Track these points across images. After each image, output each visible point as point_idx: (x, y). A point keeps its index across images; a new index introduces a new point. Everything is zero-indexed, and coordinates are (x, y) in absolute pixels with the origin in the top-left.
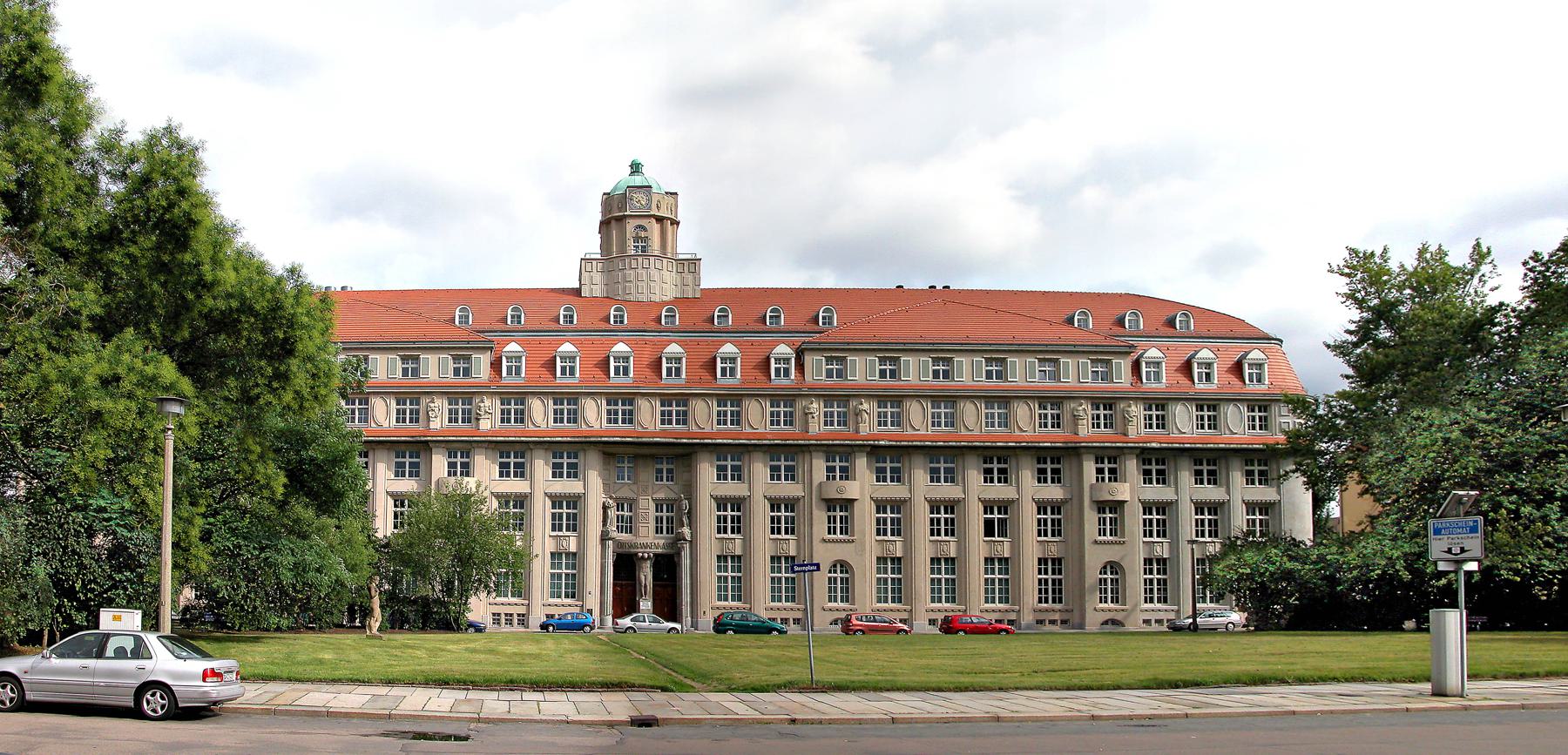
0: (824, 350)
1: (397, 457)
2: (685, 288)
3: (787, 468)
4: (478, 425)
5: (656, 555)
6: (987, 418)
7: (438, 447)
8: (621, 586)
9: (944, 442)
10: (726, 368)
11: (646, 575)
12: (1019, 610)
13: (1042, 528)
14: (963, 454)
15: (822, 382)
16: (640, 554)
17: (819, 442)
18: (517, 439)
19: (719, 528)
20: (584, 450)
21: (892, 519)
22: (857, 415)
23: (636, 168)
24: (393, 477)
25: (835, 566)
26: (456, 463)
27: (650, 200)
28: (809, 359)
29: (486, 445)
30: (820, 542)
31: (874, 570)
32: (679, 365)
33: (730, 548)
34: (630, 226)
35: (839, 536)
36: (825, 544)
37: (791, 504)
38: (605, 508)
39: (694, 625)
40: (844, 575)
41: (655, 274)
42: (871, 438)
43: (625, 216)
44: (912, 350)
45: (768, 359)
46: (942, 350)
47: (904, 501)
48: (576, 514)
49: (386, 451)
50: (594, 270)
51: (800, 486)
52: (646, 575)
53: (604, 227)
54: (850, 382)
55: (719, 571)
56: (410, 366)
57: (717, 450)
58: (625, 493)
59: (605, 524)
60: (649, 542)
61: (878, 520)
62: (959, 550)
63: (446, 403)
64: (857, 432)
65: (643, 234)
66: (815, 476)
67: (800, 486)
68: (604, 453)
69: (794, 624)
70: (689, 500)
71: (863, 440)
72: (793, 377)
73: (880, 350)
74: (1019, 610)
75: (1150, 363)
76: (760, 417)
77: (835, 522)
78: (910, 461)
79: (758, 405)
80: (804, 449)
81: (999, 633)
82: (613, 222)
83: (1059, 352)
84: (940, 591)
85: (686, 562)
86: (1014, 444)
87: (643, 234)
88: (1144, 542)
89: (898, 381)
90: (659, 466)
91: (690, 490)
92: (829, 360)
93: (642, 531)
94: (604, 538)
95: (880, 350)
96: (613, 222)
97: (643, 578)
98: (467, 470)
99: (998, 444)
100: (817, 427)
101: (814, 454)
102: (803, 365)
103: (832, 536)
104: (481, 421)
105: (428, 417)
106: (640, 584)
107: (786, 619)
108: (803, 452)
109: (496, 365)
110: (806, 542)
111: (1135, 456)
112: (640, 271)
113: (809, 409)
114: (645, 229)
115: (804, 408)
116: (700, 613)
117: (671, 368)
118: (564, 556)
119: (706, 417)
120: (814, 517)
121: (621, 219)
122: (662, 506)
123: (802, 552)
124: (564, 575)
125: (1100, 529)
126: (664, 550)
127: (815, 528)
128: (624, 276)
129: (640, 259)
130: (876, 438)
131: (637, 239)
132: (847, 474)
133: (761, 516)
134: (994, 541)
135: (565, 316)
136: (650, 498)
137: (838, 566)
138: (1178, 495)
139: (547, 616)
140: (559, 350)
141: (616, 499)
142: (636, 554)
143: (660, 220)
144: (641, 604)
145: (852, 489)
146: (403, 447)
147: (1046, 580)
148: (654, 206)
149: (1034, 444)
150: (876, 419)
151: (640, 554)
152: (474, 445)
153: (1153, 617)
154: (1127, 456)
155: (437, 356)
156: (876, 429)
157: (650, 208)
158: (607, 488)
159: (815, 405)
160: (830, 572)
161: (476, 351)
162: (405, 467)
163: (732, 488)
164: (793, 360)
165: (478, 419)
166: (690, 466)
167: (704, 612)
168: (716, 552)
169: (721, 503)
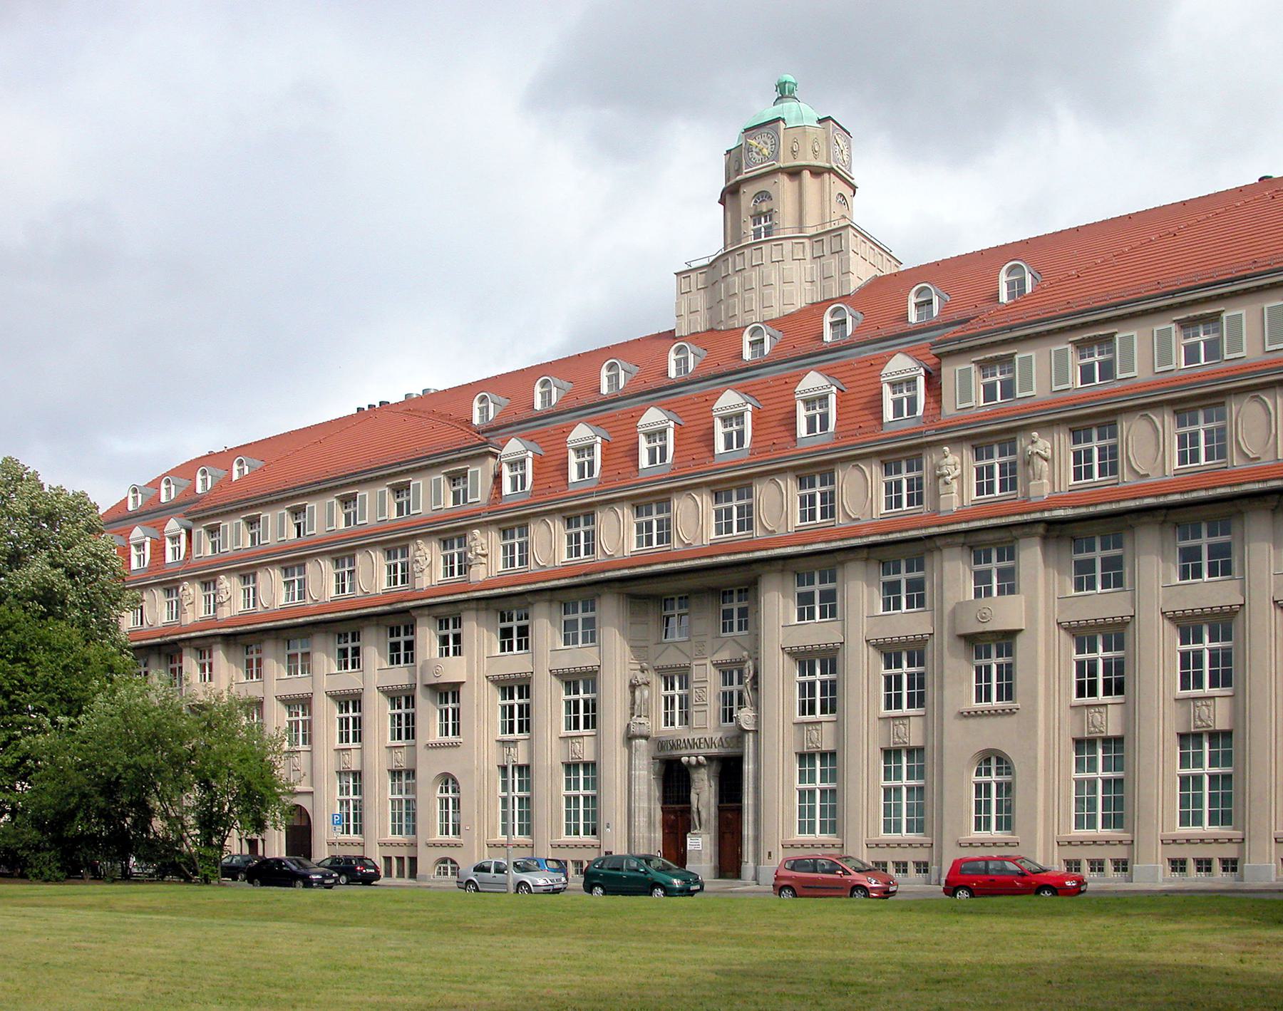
0: (971, 350)
1: (800, 584)
2: (787, 287)
3: (1215, 551)
8: (674, 812)
11: (704, 793)
13: (983, 684)
19: (1184, 677)
28: (950, 373)
29: (865, 553)
30: (955, 718)
33: (577, 751)
36: (965, 721)
37: (916, 650)
44: (1133, 316)
48: (835, 681)
49: (1157, 527)
52: (704, 793)
56: (1201, 338)
58: (671, 658)
63: (968, 454)
69: (1199, 870)
70: (756, 660)
71: (1087, 506)
73: (1073, 328)
79: (267, 574)
80: (929, 544)
81: (1037, 892)
83: (408, 472)
84: (1092, 806)
85: (748, 767)
90: (726, 606)
92: (984, 366)
95: (1073, 328)
96: (806, 174)
98: (1009, 584)
103: (984, 705)
111: (1037, 540)
112: (787, 265)
116: (763, 855)
117: (901, 400)
120: (947, 672)
122: (673, 678)
124: (904, 790)
125: (458, 720)
126: (730, 750)
127: (947, 693)
128: (762, 278)
136: (708, 662)
137: (993, 761)
139: (1068, 862)
140: (571, 438)
141: (658, 670)
144: (688, 839)
146: (573, 594)
147: (400, 801)
151: (684, 759)
153: (1190, 853)
154: (946, 552)
155: (1257, 307)
158: (638, 650)
159: (955, 458)
161: (1122, 325)
163: (819, 632)
167: (770, 853)
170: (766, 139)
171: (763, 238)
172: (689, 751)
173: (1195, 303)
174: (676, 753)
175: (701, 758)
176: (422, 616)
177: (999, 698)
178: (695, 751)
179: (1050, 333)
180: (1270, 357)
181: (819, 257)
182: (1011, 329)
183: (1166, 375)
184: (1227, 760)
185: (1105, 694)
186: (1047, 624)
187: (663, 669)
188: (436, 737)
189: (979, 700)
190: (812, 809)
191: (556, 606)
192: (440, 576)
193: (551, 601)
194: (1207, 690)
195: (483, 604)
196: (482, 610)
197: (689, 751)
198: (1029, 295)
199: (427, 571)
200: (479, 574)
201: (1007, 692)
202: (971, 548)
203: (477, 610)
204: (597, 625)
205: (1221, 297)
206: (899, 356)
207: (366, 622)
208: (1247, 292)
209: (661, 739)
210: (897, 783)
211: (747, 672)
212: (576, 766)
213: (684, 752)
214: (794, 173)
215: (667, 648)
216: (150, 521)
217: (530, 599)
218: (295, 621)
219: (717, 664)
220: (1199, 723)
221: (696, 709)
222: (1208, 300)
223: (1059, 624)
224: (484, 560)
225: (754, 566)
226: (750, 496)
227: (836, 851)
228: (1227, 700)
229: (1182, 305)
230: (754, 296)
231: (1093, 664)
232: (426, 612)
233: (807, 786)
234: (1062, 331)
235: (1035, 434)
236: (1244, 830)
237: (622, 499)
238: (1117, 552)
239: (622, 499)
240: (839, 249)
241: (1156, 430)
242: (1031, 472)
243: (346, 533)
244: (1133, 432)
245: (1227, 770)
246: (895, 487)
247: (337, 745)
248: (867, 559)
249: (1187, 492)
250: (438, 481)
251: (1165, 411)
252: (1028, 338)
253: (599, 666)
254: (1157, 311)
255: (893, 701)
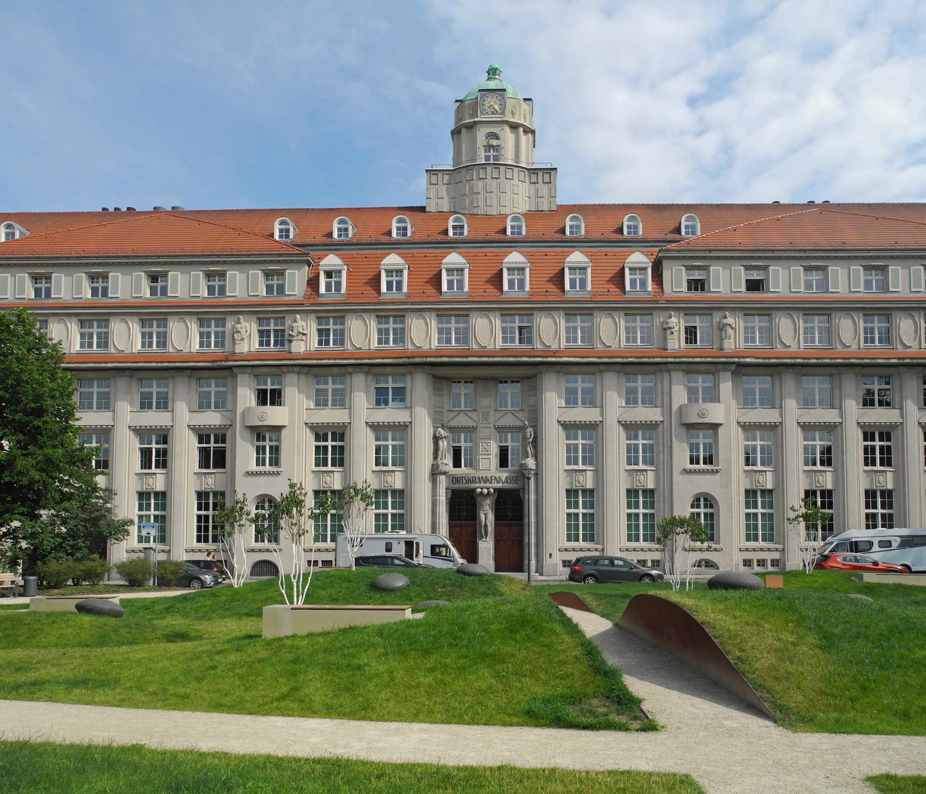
0: (684, 258)
2: (488, 195)
4: (290, 347)
5: (499, 491)
6: (866, 333)
7: (243, 373)
9: (817, 359)
10: (635, 280)
11: (487, 515)
12: (784, 549)
14: (840, 374)
15: (802, 295)
16: (479, 490)
17: (677, 360)
18: (160, 364)
19: (568, 458)
20: (411, 373)
21: (882, 448)
22: (721, 330)
23: (492, 72)
24: (312, 406)
25: (698, 500)
26: (697, 388)
27: (503, 106)
30: (243, 475)
31: (743, 504)
32: (584, 276)
34: (481, 134)
35: (702, 466)
38: (436, 439)
39: (540, 570)
40: (709, 510)
41: (507, 185)
42: (736, 355)
43: (475, 123)
45: (622, 272)
46: (152, 263)
47: (895, 426)
50: (440, 183)
51: (658, 410)
52: (487, 515)
53: (455, 136)
54: (830, 295)
55: (747, 507)
57: (562, 368)
59: (435, 457)
60: (489, 475)
61: (866, 448)
62: (896, 480)
64: (722, 349)
65: (494, 142)
66: (674, 399)
67: (658, 410)
68: (435, 377)
72: (650, 288)
74: (784, 549)
75: (635, 269)
76: (792, 334)
77: (264, 453)
78: (840, 380)
80: (662, 367)
82: (463, 130)
84: (756, 528)
86: (896, 361)
87: (494, 142)
88: (864, 471)
89: (826, 292)
91: (535, 417)
93: (483, 464)
94: (435, 473)
96: (463, 130)
97: (483, 517)
99: (879, 361)
100: (677, 343)
101: (674, 374)
102: (661, 275)
104: (294, 343)
105: (234, 340)
106: (480, 523)
107: (750, 561)
108: (662, 371)
109: (313, 283)
110: (665, 474)
111: (730, 374)
112: (488, 181)
113: (667, 323)
114: (497, 138)
115: (663, 323)
118: (152, 496)
119: (552, 333)
121: (471, 127)
123: (661, 484)
129: (489, 169)
130: (741, 354)
131: (489, 147)
132: (713, 396)
133: (616, 443)
134: (816, 471)
135: (398, 229)
137: (702, 500)
138: (603, 417)
142: (474, 490)
143: (514, 127)
145: (715, 413)
147: (207, 517)
148: (508, 112)
149: (919, 361)
150: (742, 335)
152: (285, 369)
153: (755, 556)
156: (742, 345)
157: (503, 113)
159: (674, 320)
160: (692, 506)
162: (92, 398)
164: (650, 270)
165: (290, 341)
166: (535, 388)
167: (551, 555)
168: (564, 484)
169: (569, 428)
170: (495, 100)
171: (492, 162)
172: (482, 485)
173: (815, 258)
174: (473, 486)
175: (492, 490)
176: (244, 373)
177: (271, 465)
178: (488, 485)
179: (732, 258)
180: (17, 301)
181: (535, 183)
182: (710, 251)
183: (195, 299)
184: (164, 508)
185: (156, 468)
186: (299, 423)
187: (502, 427)
188: (253, 467)
189: (258, 464)
190: (637, 526)
191: (370, 378)
192: (256, 346)
193: (367, 373)
194: (390, 467)
195: (305, 370)
196: (304, 374)
197: (482, 485)
198: (17, 240)
199: (246, 341)
200: (729, 345)
201: (275, 462)
202: (256, 376)
203: (299, 373)
204: (112, 398)
205: (711, 258)
206: (515, 253)
207: (180, 373)
208: (725, 258)
209: (456, 476)
210: (148, 513)
211: (529, 434)
212: (149, 494)
213: (477, 485)
214: (514, 127)
215: (455, 417)
216: (587, 249)
217: (350, 370)
218: (198, 364)
219: (498, 427)
220: (325, 485)
221: (481, 457)
222: (822, 258)
223: (129, 427)
224: (304, 338)
225: (540, 367)
226: (165, 326)
227: (597, 554)
228: (163, 476)
229: (808, 258)
230: (494, 196)
231: (873, 448)
232: (249, 370)
233: (633, 511)
234: (739, 258)
235: (298, 316)
236: (603, 545)
237: (430, 310)
238: (224, 389)
239: (430, 310)
240: (548, 181)
241: (187, 328)
242: (724, 335)
243: (90, 302)
244: (175, 328)
245: (401, 511)
246: (869, 331)
247: (138, 469)
248: (619, 372)
249: (820, 358)
250: (139, 277)
251: (309, 318)
252: (718, 258)
253: (411, 422)
254: (794, 258)
255: (146, 464)
